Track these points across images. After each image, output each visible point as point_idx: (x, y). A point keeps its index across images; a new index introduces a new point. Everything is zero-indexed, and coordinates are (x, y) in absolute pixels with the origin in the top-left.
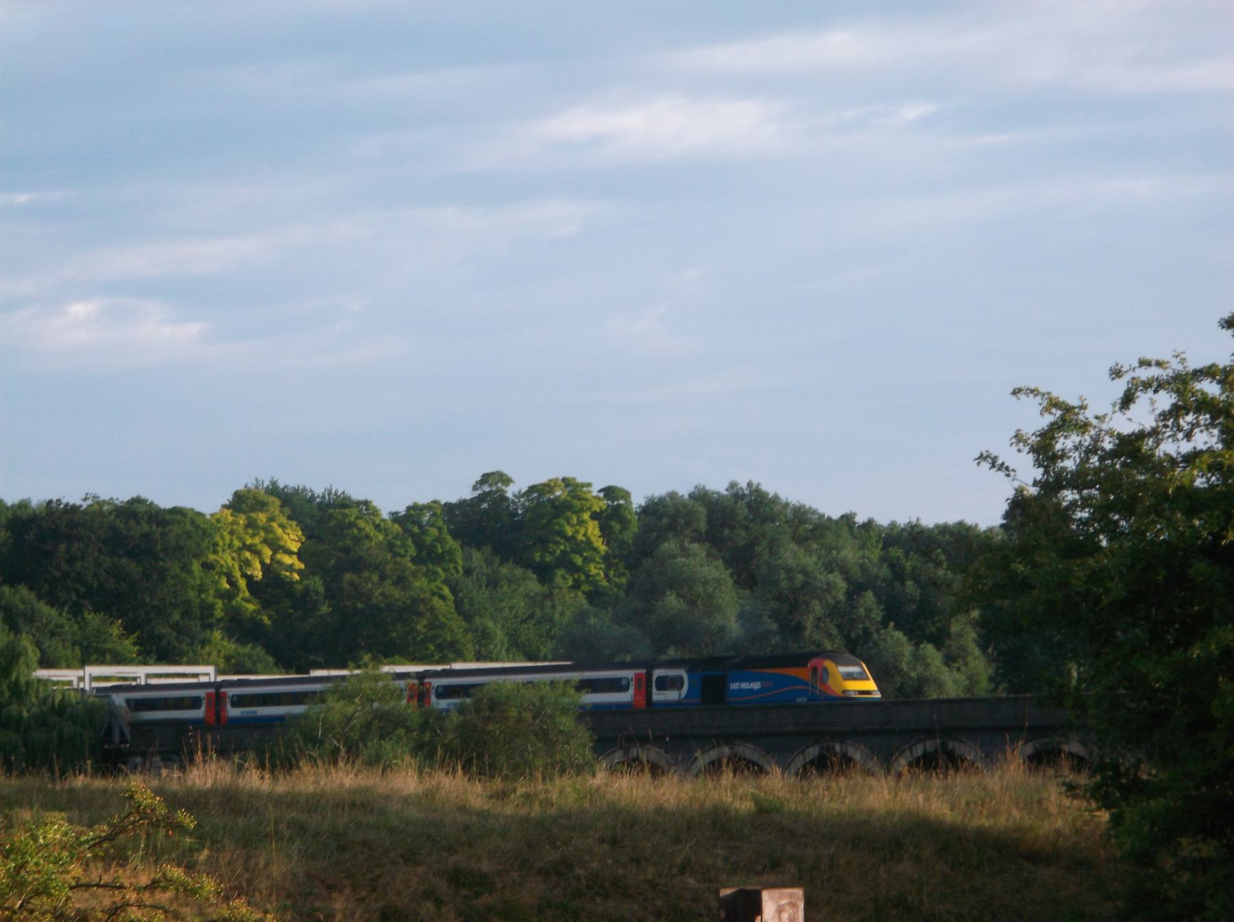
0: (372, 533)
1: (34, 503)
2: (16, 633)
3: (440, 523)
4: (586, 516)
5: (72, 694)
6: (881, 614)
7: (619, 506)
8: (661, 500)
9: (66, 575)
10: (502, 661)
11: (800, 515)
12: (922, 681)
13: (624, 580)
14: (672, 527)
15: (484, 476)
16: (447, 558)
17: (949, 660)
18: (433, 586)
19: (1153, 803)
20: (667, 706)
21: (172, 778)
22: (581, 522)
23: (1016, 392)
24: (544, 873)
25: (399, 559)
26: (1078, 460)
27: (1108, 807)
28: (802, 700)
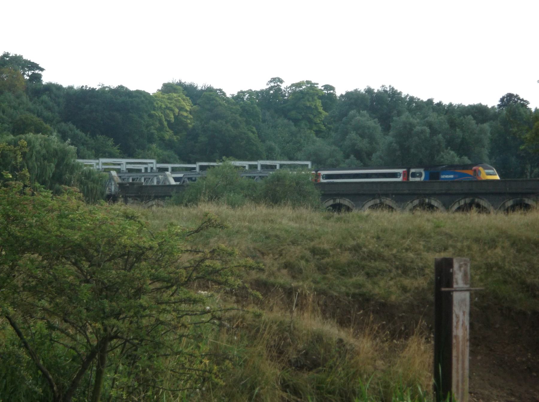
1: (75, 88)
4: (316, 98)
7: (331, 94)
24: (350, 250)
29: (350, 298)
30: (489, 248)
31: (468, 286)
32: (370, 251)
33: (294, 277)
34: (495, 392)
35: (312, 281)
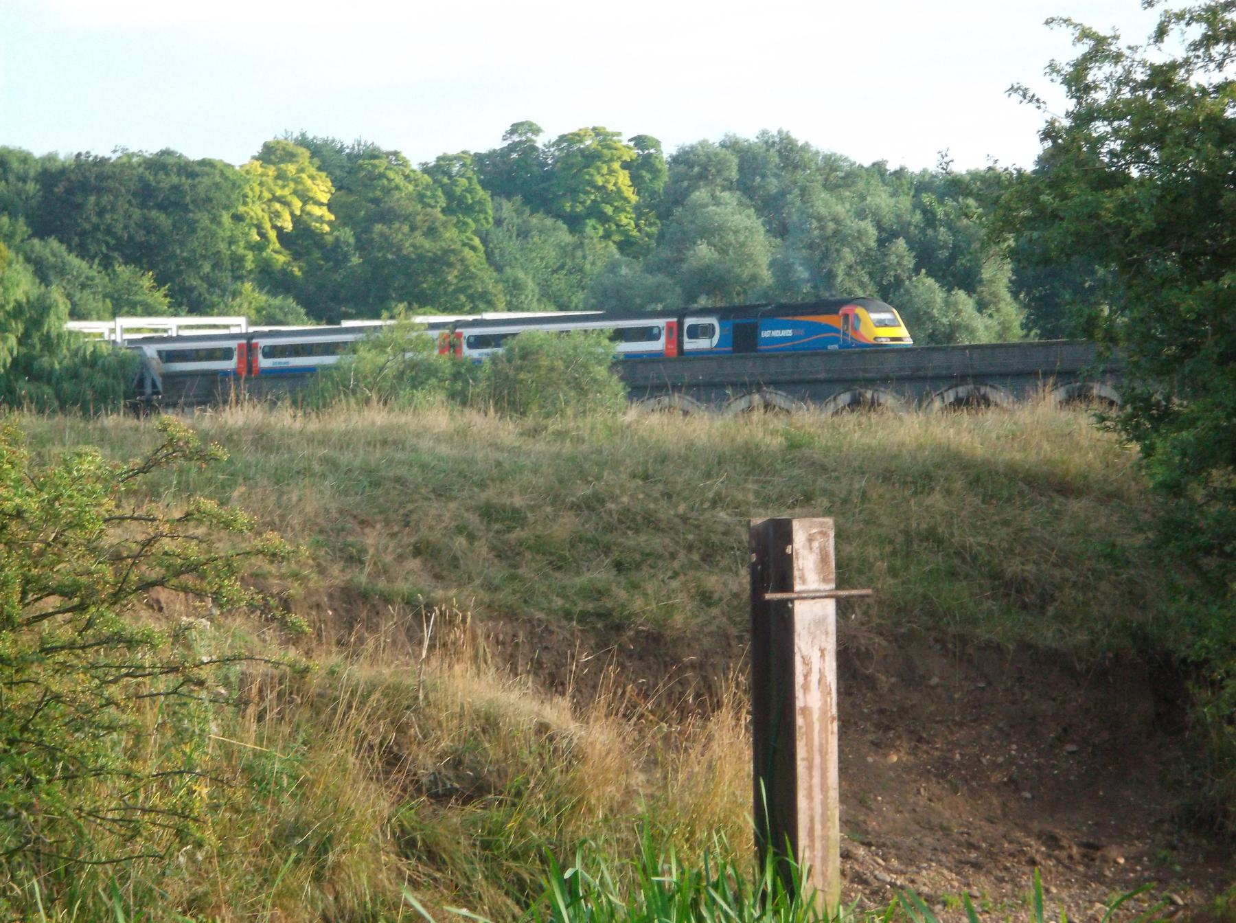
0: (401, 184)
1: (61, 157)
2: (47, 286)
3: (470, 174)
4: (616, 165)
5: (104, 346)
6: (914, 262)
7: (650, 155)
8: (693, 149)
9: (96, 228)
10: (533, 311)
11: (831, 164)
12: (954, 328)
13: (654, 229)
14: (703, 176)
15: (513, 125)
16: (477, 209)
17: (981, 306)
18: (463, 237)
19: (1184, 434)
20: (699, 354)
21: (207, 419)
22: (611, 172)
23: (1048, 22)
24: (576, 507)
25: (429, 209)
26: (1109, 91)
27: (1138, 439)
28: (833, 347)
29: (574, 623)
30: (915, 493)
31: (832, 586)
32: (626, 511)
33: (438, 577)
34: (929, 840)
35: (482, 586)
